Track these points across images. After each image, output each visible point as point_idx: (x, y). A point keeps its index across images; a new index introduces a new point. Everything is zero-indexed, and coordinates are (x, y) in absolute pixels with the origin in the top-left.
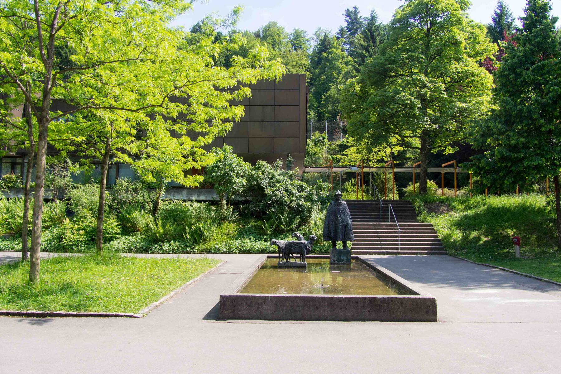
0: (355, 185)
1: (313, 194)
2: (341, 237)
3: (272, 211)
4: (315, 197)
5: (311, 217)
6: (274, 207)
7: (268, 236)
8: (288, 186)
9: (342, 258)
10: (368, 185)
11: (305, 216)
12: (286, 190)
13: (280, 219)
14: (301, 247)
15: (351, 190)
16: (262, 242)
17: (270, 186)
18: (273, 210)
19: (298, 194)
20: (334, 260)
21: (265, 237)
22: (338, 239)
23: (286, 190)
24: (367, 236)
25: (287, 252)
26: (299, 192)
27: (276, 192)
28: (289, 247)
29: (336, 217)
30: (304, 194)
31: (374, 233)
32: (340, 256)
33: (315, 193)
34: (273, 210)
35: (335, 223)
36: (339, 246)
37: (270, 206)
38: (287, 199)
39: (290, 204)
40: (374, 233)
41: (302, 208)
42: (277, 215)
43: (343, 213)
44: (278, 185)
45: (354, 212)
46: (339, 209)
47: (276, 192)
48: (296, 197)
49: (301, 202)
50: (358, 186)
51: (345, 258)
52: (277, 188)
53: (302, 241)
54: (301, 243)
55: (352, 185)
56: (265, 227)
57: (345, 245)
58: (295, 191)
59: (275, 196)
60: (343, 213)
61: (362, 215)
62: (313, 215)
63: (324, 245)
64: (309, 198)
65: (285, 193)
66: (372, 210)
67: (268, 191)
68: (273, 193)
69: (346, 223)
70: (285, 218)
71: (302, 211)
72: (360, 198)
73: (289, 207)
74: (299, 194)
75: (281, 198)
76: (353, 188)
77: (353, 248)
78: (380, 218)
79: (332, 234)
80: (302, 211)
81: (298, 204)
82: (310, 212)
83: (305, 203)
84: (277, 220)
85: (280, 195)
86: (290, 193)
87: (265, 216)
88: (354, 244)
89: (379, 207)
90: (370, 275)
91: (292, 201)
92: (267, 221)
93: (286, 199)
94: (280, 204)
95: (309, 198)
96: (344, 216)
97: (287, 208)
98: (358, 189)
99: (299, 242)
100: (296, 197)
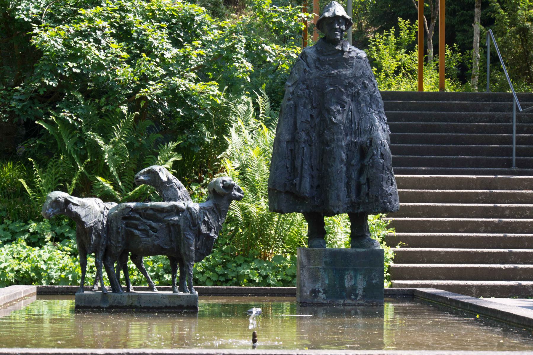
0: (410, 49)
1: (232, 50)
2: (343, 193)
3: (63, 121)
4: (244, 66)
5: (225, 146)
6: (72, 105)
7: (46, 224)
8: (130, 17)
9: (348, 283)
10: (466, 47)
11: (201, 142)
12: (123, 33)
13: (97, 151)
14: (176, 225)
15: (394, 65)
16: (21, 246)
17: (55, 19)
18: (65, 114)
19: (172, 53)
20: (315, 292)
21: (33, 226)
22: (333, 201)
23: (123, 33)
24: (455, 227)
25: (117, 246)
26: (176, 44)
27: (82, 43)
28: (122, 225)
29: (322, 111)
30: (196, 53)
31: (485, 212)
32: (340, 274)
33: (241, 48)
34: (65, 114)
35: (320, 135)
36: (339, 230)
37: (52, 99)
38: (124, 72)
39: (136, 90)
40: (485, 212)
41: (188, 108)
42: (82, 139)
43: (355, 97)
44: (90, 12)
45: (404, 140)
46: (337, 80)
47: (82, 43)
48: (164, 64)
49: (184, 83)
50: (424, 51)
51: (361, 284)
52: (84, 25)
53: (180, 204)
54: (177, 210)
55: (398, 46)
56: (31, 184)
57: (359, 231)
58: (158, 38)
59: (73, 58)
60: (355, 97)
61: (436, 152)
62: (234, 140)
63: (278, 259)
64: (216, 67)
65: (115, 46)
66: (479, 129)
67: (49, 38)
68: (66, 45)
69: (364, 138)
70: (117, 152)
71: (188, 124)
72: (429, 85)
73: (135, 104)
74: (175, 51)
75: (100, 67)
76: (402, 55)
77: (396, 274)
78: (509, 164)
79: (306, 185)
80: (188, 124)
81: (172, 90)
82: (221, 125)
83: (200, 87)
84: (82, 159)
85: (95, 54)
86: (138, 47)
87: (34, 143)
88: (399, 258)
89: (508, 119)
90: (467, 328)
91: (144, 79)
92: (43, 165)
93: (119, 71)
94: (99, 92)
95: (216, 67)
96: (359, 111)
97: (124, 109)
98: (424, 61)
99: (166, 204)
100: (164, 64)
